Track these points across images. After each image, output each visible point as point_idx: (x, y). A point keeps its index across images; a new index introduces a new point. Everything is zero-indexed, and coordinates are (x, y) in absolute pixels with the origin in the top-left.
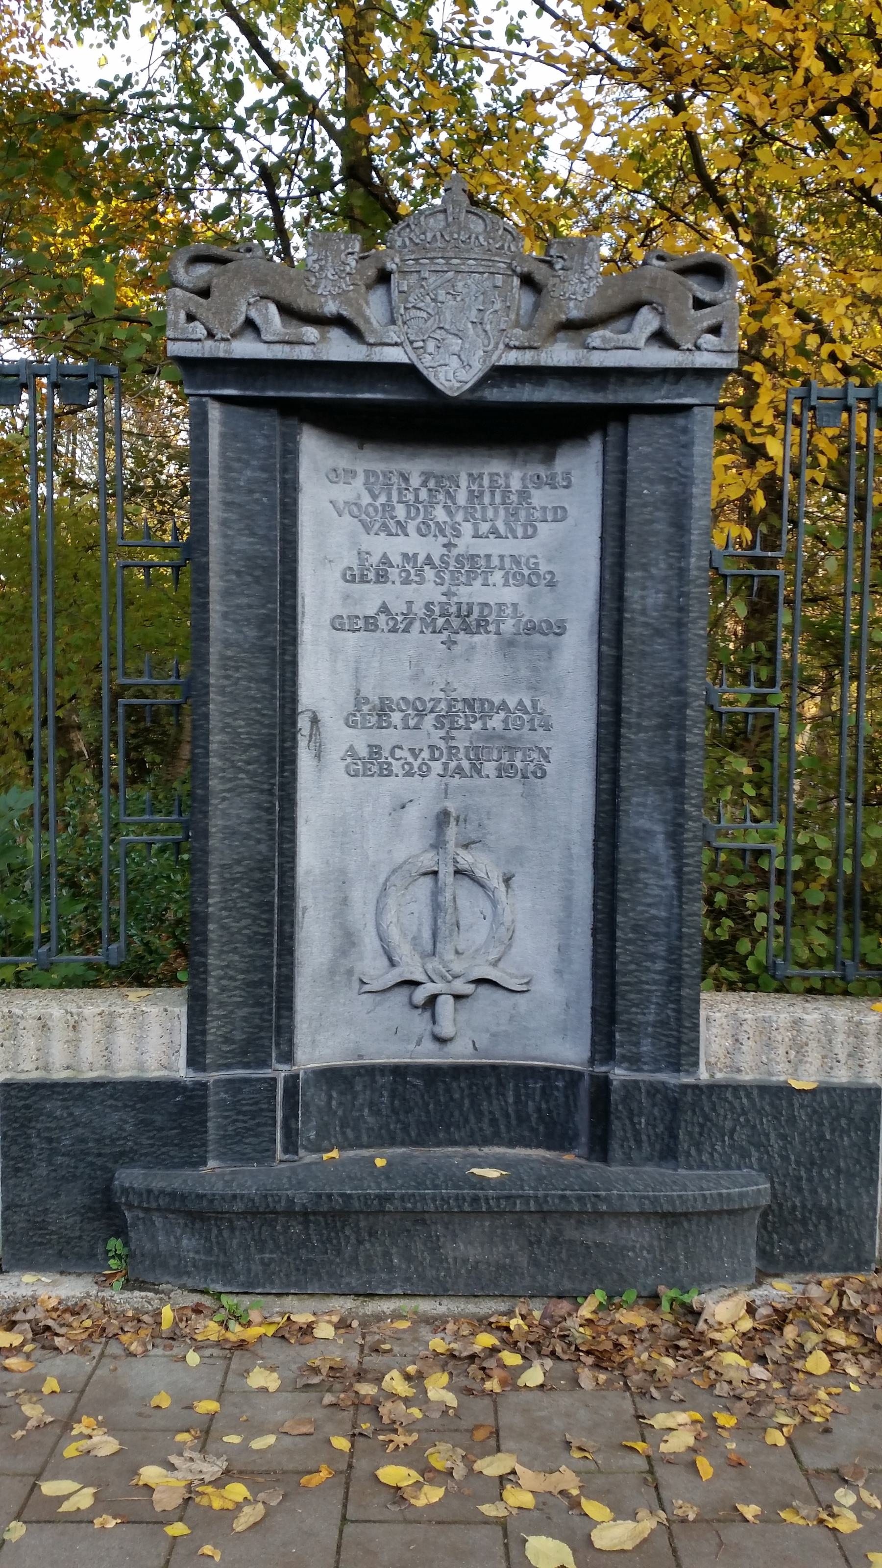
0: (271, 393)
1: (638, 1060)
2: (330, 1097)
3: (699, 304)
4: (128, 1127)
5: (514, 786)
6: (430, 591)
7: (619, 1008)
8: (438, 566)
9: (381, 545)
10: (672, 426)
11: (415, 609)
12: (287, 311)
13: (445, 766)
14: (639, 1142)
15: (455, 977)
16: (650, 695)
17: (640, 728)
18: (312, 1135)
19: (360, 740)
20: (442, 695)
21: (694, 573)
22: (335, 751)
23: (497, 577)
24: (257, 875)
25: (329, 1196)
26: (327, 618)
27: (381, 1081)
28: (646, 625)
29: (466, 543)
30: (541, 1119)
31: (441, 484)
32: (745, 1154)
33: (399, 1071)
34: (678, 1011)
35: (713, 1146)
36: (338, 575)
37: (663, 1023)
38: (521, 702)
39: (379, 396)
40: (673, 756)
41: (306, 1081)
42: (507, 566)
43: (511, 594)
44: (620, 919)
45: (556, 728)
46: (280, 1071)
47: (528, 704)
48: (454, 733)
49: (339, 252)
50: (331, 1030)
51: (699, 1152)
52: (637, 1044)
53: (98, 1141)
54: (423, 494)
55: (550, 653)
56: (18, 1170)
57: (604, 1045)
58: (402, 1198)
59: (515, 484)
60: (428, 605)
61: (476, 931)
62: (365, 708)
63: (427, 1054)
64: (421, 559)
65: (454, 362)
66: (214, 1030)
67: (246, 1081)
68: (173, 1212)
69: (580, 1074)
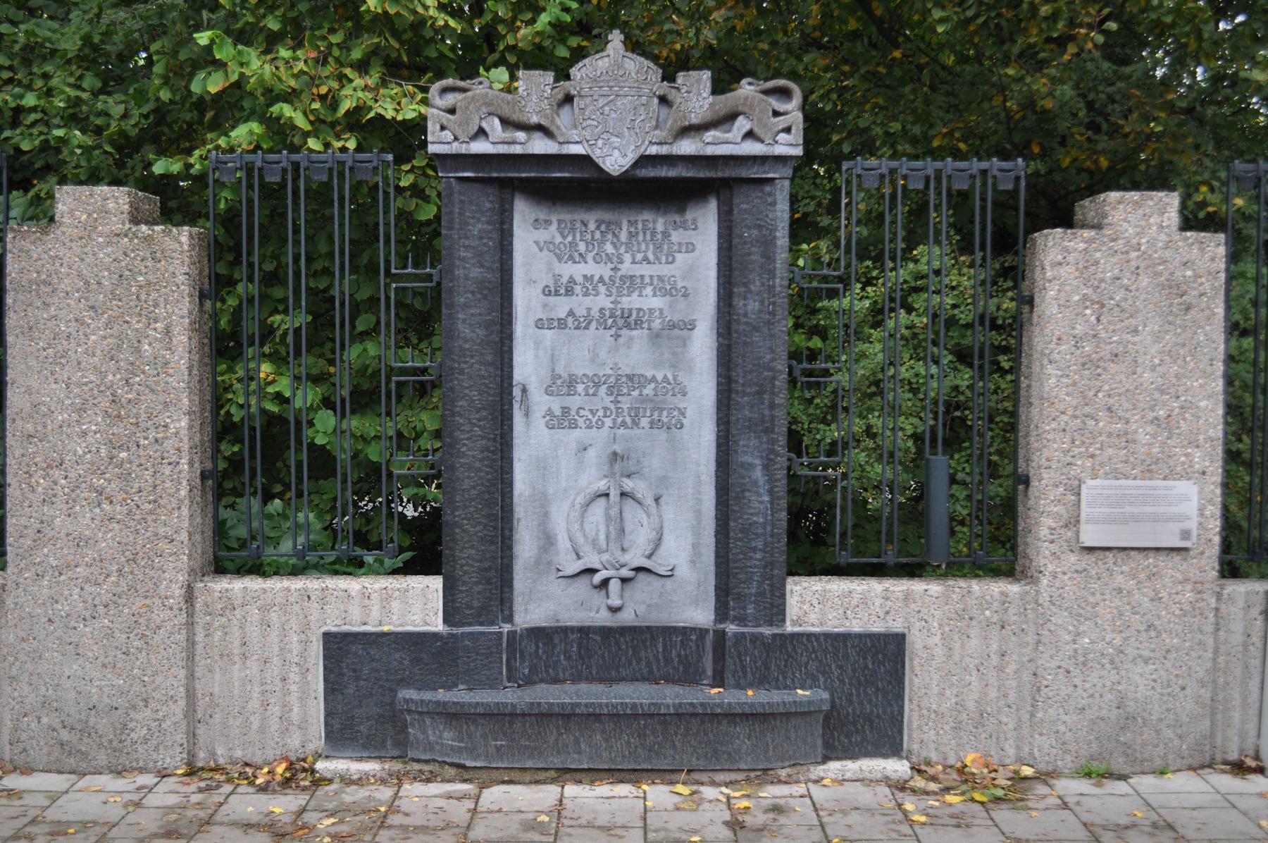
0: (495, 175)
1: (745, 619)
2: (537, 647)
3: (776, 114)
4: (406, 662)
5: (662, 435)
6: (602, 301)
7: (731, 585)
8: (609, 283)
9: (568, 270)
10: (762, 191)
11: (592, 313)
12: (505, 122)
13: (614, 420)
14: (745, 673)
15: (622, 566)
16: (751, 372)
17: (744, 394)
18: (526, 671)
19: (556, 405)
20: (611, 372)
21: (778, 289)
22: (538, 412)
23: (649, 290)
24: (487, 496)
25: (539, 704)
26: (532, 321)
27: (572, 637)
28: (748, 323)
29: (626, 268)
30: (680, 662)
31: (609, 227)
32: (815, 679)
33: (584, 631)
34: (771, 585)
35: (793, 674)
36: (539, 291)
37: (761, 594)
38: (665, 377)
39: (566, 175)
40: (767, 412)
41: (521, 635)
42: (655, 282)
43: (656, 303)
44: (732, 524)
45: (690, 394)
46: (506, 628)
47: (670, 377)
48: (620, 398)
49: (540, 84)
50: (541, 602)
51: (785, 678)
52: (745, 608)
53: (386, 671)
54: (598, 235)
55: (684, 342)
56: (334, 690)
57: (722, 612)
58: (586, 705)
59: (660, 227)
60: (601, 310)
61: (640, 539)
62: (559, 382)
63: (602, 618)
64: (596, 278)
65: (616, 153)
66: (462, 598)
67: (482, 633)
68: (438, 714)
69: (707, 631)
